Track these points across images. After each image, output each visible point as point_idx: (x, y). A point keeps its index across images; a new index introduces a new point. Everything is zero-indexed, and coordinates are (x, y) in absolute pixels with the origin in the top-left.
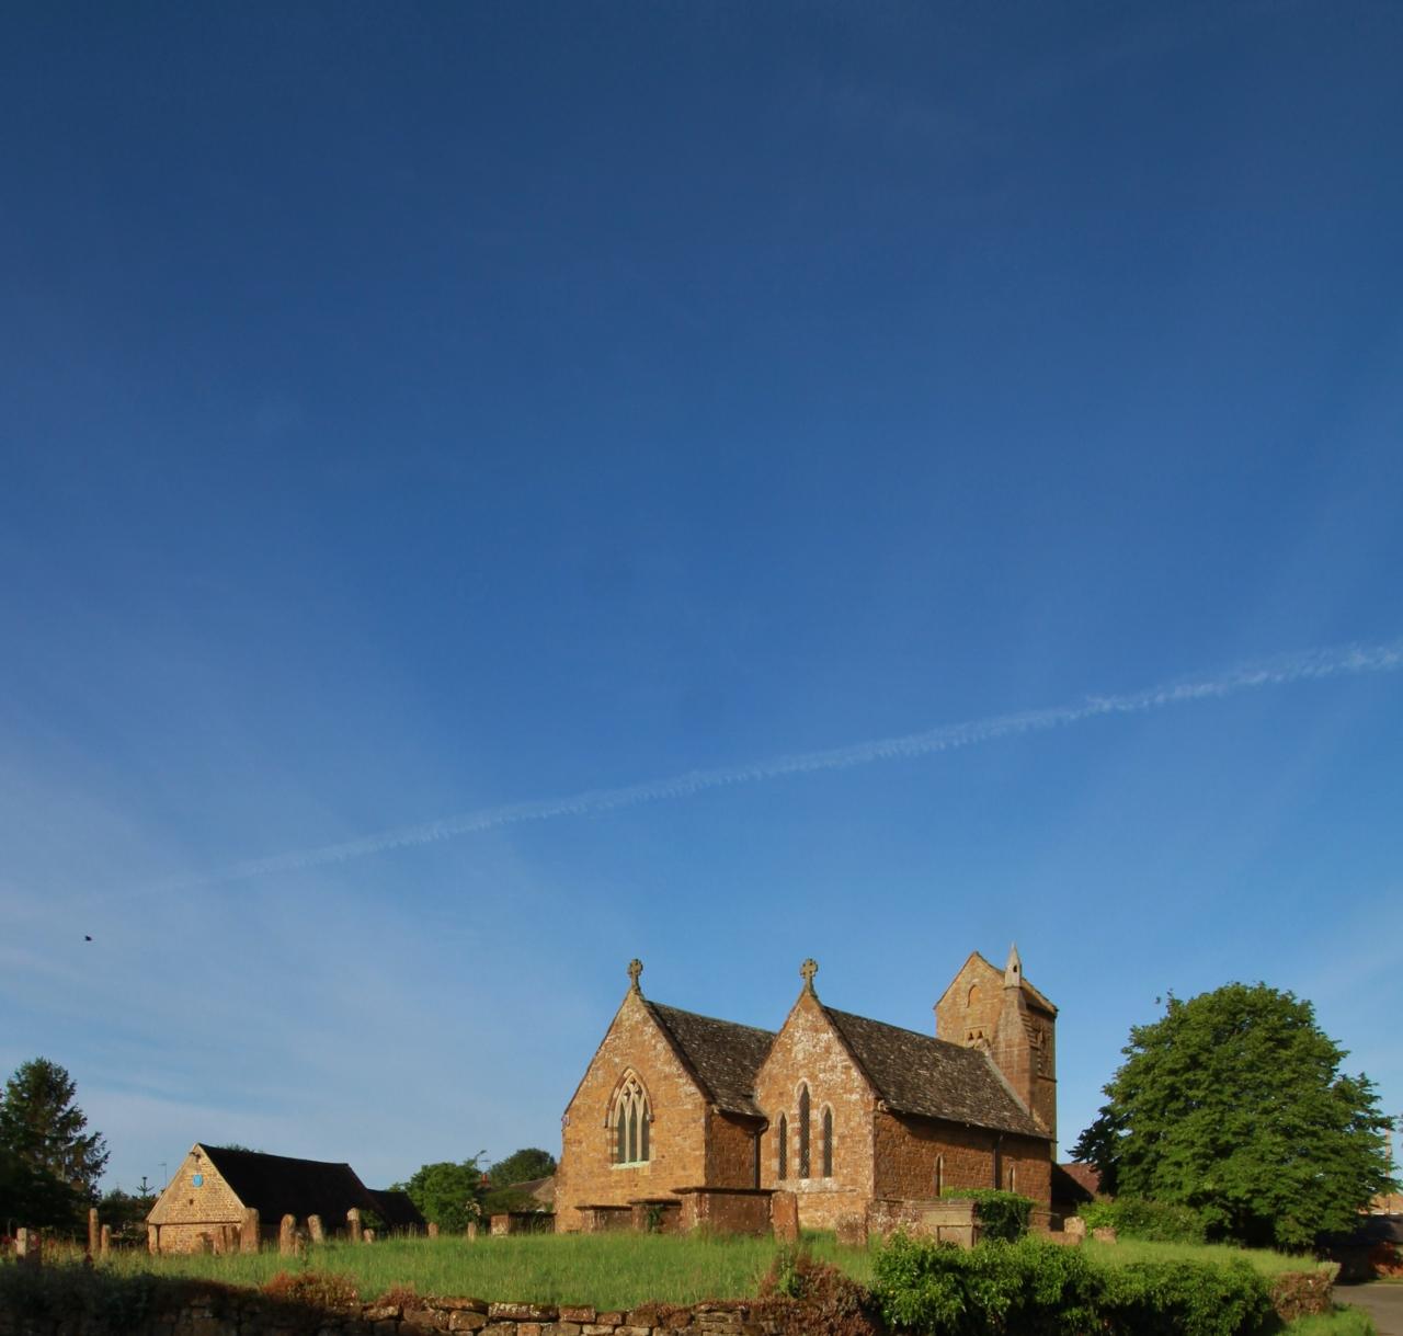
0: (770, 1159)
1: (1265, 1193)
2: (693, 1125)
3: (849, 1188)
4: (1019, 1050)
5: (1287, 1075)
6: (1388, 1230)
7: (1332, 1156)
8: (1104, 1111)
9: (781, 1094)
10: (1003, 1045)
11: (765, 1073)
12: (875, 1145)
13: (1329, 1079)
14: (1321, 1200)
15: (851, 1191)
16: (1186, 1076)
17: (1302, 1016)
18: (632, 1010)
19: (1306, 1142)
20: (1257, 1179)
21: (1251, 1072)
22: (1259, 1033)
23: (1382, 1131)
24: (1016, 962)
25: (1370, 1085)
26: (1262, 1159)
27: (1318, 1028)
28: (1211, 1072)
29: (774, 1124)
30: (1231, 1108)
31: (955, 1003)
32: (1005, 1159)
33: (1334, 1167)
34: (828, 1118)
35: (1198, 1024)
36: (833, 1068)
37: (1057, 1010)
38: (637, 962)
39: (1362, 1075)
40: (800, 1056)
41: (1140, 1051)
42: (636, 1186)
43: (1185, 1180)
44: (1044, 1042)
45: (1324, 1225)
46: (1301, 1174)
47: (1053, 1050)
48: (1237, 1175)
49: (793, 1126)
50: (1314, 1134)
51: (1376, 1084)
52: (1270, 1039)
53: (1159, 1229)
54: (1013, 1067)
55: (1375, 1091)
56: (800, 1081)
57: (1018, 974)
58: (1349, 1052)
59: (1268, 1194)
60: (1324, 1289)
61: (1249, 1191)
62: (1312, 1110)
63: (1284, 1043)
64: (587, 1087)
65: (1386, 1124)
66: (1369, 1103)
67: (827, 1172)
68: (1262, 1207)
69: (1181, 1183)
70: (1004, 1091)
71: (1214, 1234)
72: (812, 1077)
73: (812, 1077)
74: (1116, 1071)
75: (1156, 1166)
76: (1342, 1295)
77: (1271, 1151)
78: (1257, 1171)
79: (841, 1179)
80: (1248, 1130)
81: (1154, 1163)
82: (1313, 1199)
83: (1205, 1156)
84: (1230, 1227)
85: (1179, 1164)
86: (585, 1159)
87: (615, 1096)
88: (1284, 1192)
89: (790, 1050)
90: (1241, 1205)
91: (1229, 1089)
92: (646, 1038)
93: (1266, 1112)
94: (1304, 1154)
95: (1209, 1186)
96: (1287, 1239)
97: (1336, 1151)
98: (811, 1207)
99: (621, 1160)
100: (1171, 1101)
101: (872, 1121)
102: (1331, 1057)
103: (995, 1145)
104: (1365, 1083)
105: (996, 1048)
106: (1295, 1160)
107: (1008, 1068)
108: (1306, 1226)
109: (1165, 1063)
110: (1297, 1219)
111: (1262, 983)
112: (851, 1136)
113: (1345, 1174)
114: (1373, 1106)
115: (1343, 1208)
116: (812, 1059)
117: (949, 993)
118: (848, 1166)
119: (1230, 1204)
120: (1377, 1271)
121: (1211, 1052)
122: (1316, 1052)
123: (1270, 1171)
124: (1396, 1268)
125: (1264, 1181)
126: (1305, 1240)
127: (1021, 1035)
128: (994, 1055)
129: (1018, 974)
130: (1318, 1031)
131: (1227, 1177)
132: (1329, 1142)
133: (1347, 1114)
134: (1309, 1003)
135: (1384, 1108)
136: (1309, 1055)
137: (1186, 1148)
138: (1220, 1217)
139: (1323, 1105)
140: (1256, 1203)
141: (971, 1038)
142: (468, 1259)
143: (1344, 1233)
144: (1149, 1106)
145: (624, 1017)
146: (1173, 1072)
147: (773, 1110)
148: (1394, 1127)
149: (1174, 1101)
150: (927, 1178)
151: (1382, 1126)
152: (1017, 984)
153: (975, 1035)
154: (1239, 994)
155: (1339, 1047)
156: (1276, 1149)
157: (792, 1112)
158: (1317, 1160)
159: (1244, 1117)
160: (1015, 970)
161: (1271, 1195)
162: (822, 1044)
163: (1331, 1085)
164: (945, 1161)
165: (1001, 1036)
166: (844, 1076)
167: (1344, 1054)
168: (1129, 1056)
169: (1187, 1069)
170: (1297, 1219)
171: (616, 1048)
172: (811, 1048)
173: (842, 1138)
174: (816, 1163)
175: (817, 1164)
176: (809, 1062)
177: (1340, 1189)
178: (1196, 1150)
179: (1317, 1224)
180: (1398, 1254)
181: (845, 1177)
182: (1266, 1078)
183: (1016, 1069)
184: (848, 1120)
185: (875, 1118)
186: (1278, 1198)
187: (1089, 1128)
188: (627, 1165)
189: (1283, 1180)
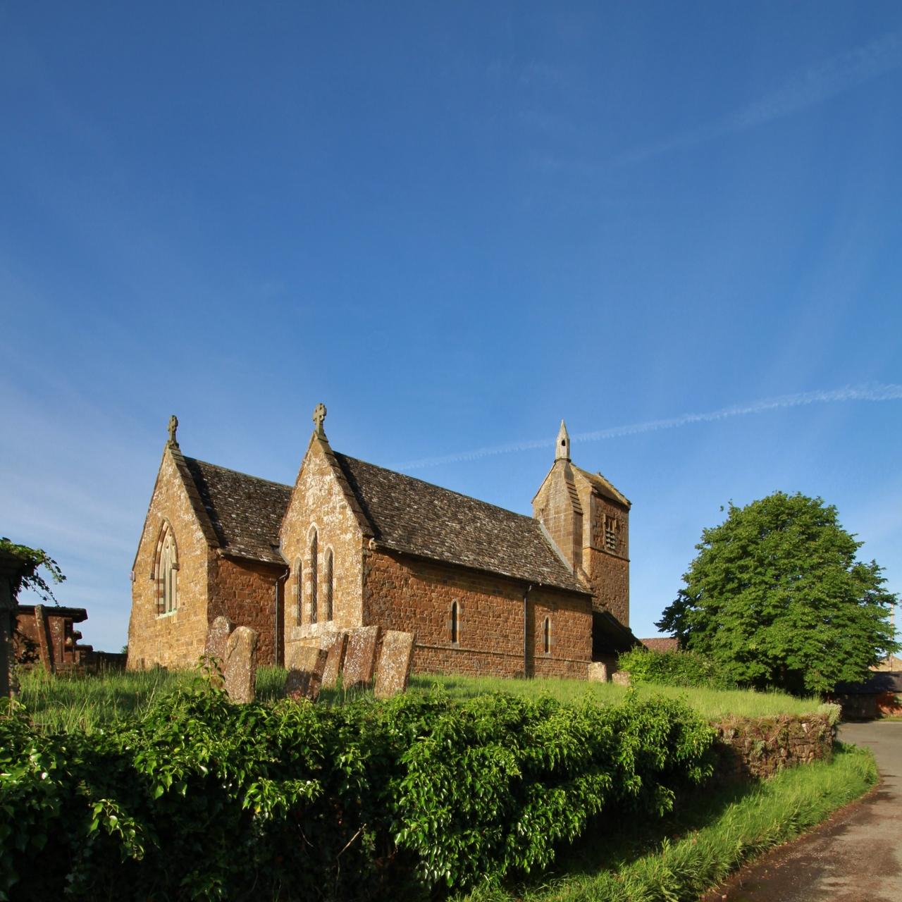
1: (797, 652)
4: (565, 516)
5: (815, 560)
6: (892, 683)
7: (849, 623)
8: (682, 592)
10: (552, 512)
11: (287, 522)
12: (365, 584)
13: (848, 565)
14: (840, 658)
16: (739, 563)
17: (827, 518)
19: (830, 613)
20: (790, 641)
21: (788, 559)
22: (795, 528)
23: (887, 605)
24: (564, 437)
25: (879, 570)
26: (795, 626)
27: (841, 526)
28: (756, 559)
30: (771, 586)
32: (539, 610)
33: (850, 631)
35: (748, 522)
37: (630, 503)
38: (173, 416)
39: (874, 562)
41: (708, 547)
43: (734, 642)
44: (618, 527)
45: (842, 677)
46: (824, 637)
47: (626, 535)
48: (776, 638)
49: (307, 571)
50: (835, 605)
51: (884, 569)
52: (803, 533)
53: (685, 675)
54: (560, 531)
55: (883, 575)
57: (565, 447)
58: (863, 543)
59: (799, 653)
60: (820, 733)
61: (783, 651)
62: (833, 587)
63: (812, 537)
65: (891, 599)
66: (879, 583)
67: (330, 616)
68: (794, 663)
69: (731, 644)
70: (552, 552)
71: (760, 684)
72: (320, 526)
73: (320, 526)
74: (691, 562)
75: (716, 633)
76: (850, 734)
77: (802, 620)
78: (790, 635)
80: (784, 602)
81: (715, 630)
82: (834, 656)
83: (753, 625)
84: (770, 678)
85: (729, 630)
87: (159, 549)
88: (811, 651)
90: (779, 662)
91: (771, 571)
93: (798, 589)
94: (828, 621)
95: (753, 646)
96: (814, 687)
97: (852, 620)
100: (728, 583)
101: (361, 560)
102: (848, 548)
103: (526, 595)
104: (876, 569)
105: (548, 515)
106: (821, 626)
107: (556, 532)
108: (828, 677)
109: (724, 554)
110: (821, 672)
111: (799, 494)
113: (859, 637)
114: (881, 586)
115: (856, 664)
117: (543, 489)
119: (770, 661)
120: (881, 711)
121: (757, 544)
122: (838, 543)
123: (800, 635)
124: (895, 709)
125: (796, 642)
126: (827, 688)
127: (567, 502)
128: (546, 521)
129: (565, 447)
130: (840, 529)
131: (768, 640)
132: (847, 612)
133: (862, 591)
134: (834, 507)
135: (890, 588)
136: (833, 545)
137: (737, 618)
138: (763, 671)
139: (842, 583)
140: (789, 660)
143: (857, 683)
144: (711, 586)
146: (730, 560)
147: (292, 558)
148: (897, 601)
149: (729, 583)
150: (439, 622)
151: (888, 601)
152: (565, 456)
154: (781, 500)
155: (856, 539)
156: (805, 618)
158: (838, 626)
159: (780, 593)
160: (563, 443)
161: (801, 653)
162: (326, 487)
163: (850, 569)
164: (462, 607)
165: (551, 505)
166: (341, 517)
167: (859, 544)
168: (701, 550)
169: (740, 558)
170: (821, 672)
172: (318, 492)
173: (340, 579)
174: (321, 607)
175: (322, 609)
176: (317, 507)
177: (855, 648)
178: (743, 621)
179: (837, 676)
180: (897, 700)
182: (799, 563)
183: (562, 532)
185: (365, 557)
186: (806, 656)
187: (670, 606)
189: (810, 641)
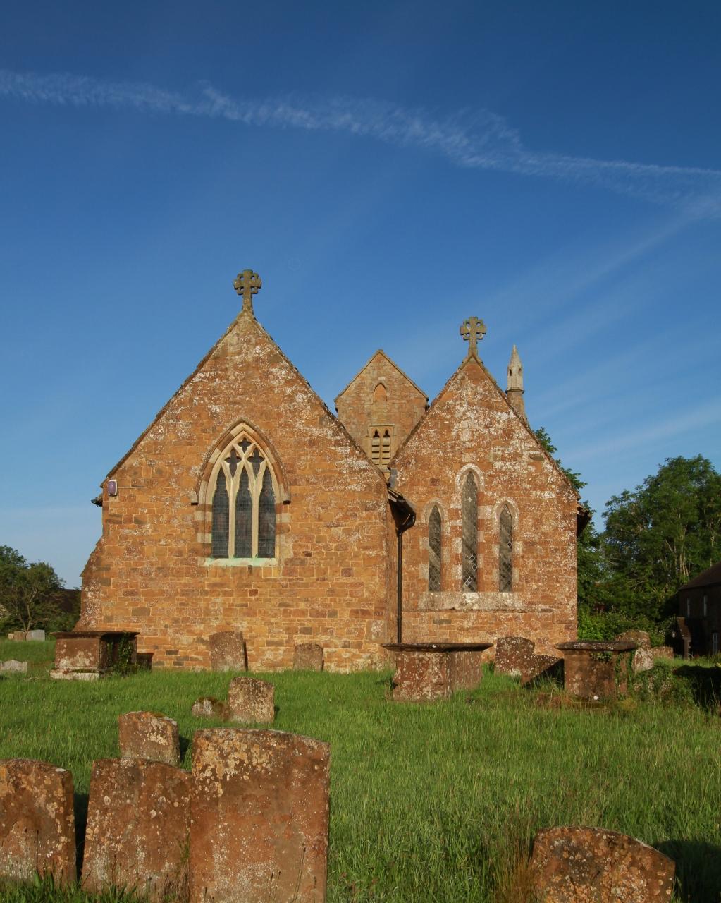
0: (417, 564)
2: (364, 514)
3: (540, 607)
9: (435, 482)
15: (543, 611)
18: (249, 342)
29: (423, 519)
31: (358, 398)
34: (505, 521)
36: (516, 457)
40: (465, 437)
42: (254, 592)
56: (466, 468)
64: (156, 443)
79: (529, 595)
86: (149, 548)
87: (211, 460)
89: (449, 428)
92: (275, 383)
98: (482, 628)
99: (219, 552)
112: (543, 543)
116: (481, 444)
117: (353, 387)
118: (539, 580)
141: (376, 435)
142: (497, 766)
145: (231, 349)
153: (381, 432)
157: (452, 506)
167: (583, 484)
171: (213, 392)
172: (482, 429)
173: (530, 544)
176: (480, 445)
181: (534, 593)
184: (538, 523)
188: (232, 562)
